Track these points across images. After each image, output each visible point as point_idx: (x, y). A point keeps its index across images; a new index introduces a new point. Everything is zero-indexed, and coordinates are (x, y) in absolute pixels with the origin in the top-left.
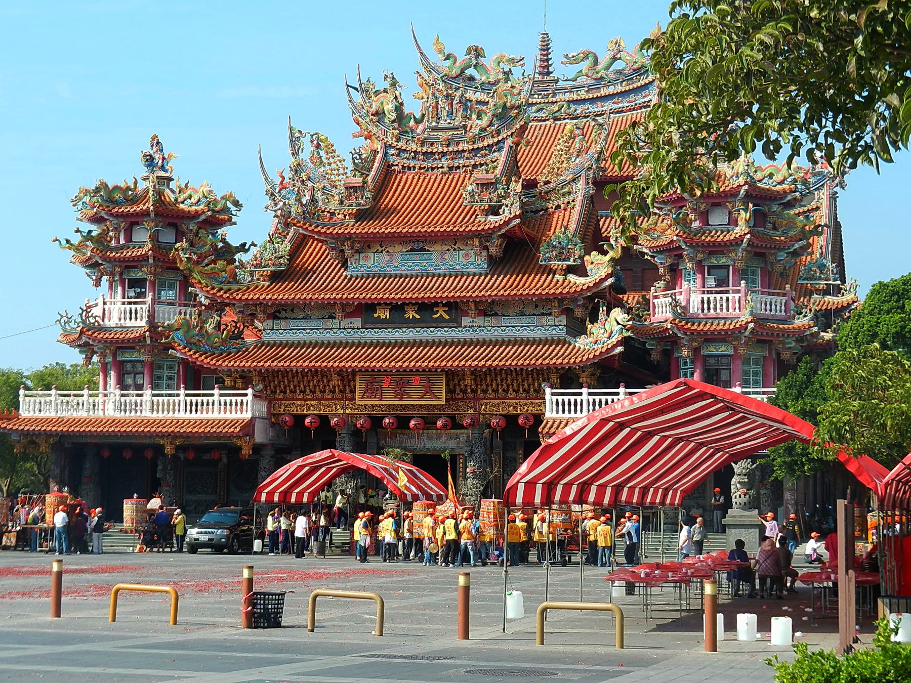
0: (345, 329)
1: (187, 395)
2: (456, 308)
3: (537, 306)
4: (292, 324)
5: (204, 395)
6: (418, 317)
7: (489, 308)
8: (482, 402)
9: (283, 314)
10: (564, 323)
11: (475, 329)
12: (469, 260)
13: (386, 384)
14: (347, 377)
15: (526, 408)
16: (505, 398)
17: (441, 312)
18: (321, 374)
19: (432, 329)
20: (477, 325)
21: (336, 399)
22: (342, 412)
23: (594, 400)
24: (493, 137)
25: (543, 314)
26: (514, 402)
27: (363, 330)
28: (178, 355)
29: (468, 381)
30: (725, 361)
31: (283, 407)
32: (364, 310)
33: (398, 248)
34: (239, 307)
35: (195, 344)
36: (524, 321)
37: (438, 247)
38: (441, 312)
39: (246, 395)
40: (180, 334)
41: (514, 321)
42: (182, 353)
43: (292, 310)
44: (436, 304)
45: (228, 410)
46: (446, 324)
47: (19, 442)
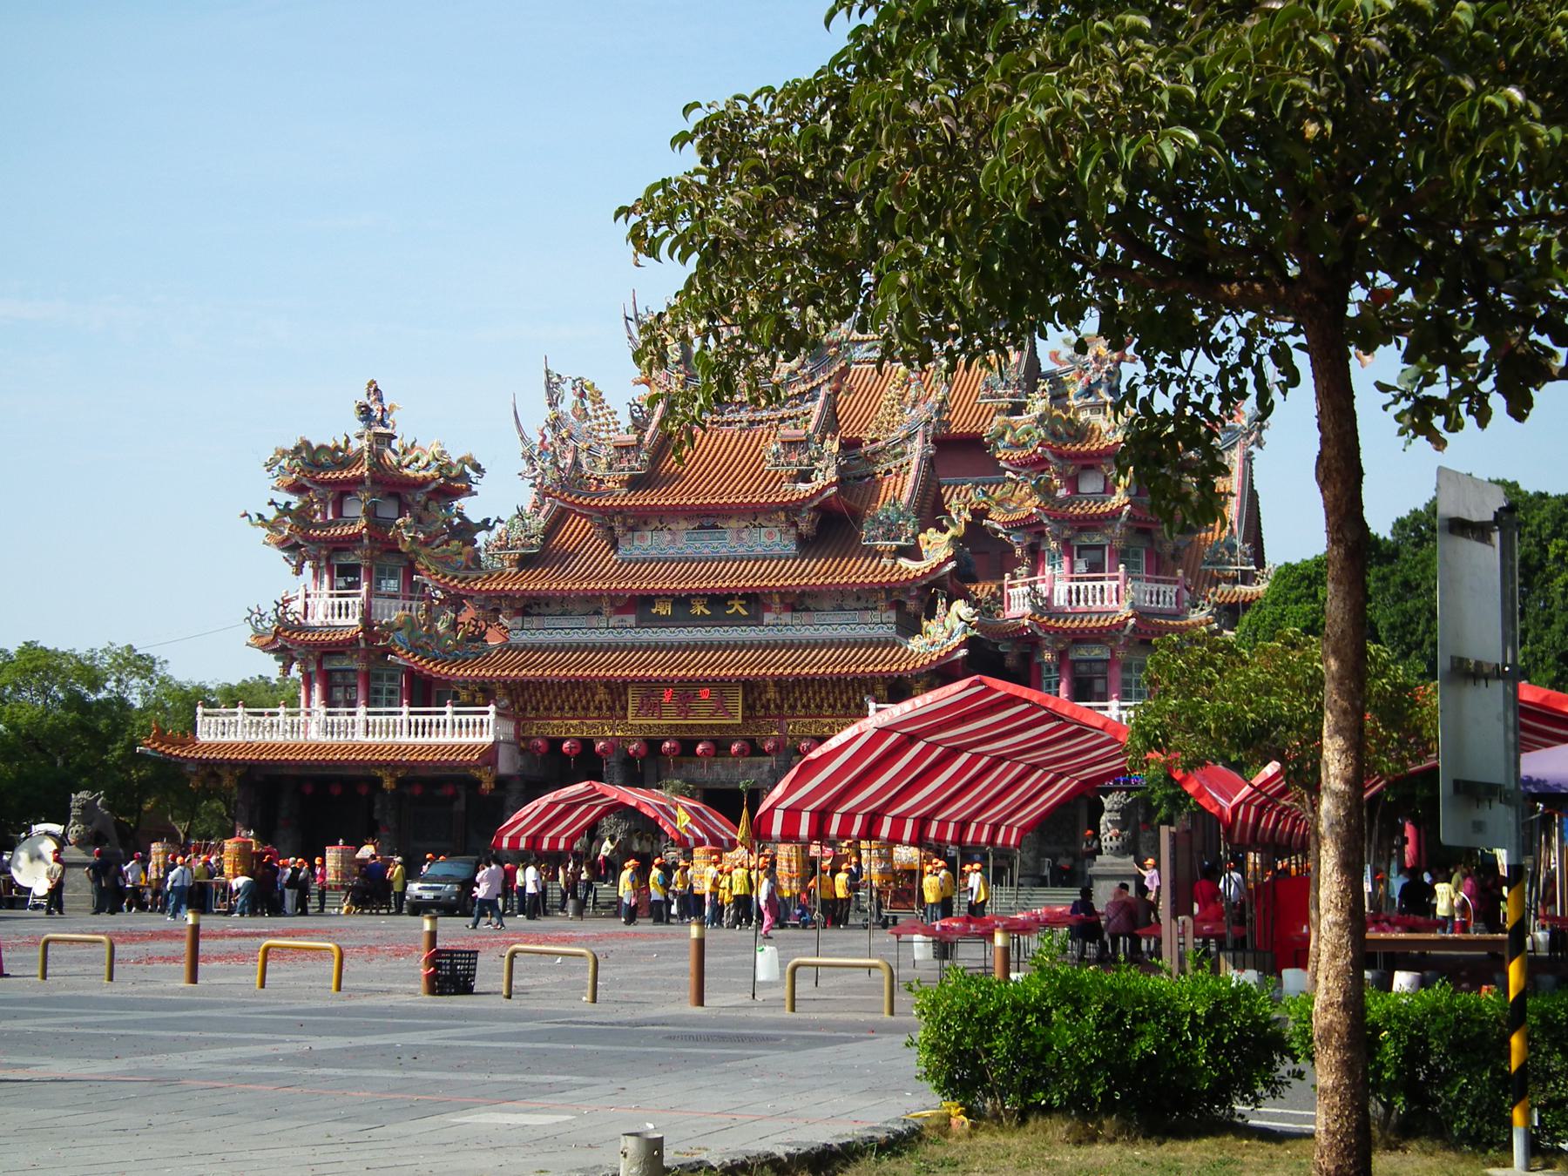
1: (412, 713)
2: (756, 601)
3: (859, 598)
4: (548, 622)
7: (798, 601)
10: (894, 619)
12: (773, 540)
17: (737, 606)
24: (805, 382)
25: (867, 609)
28: (400, 662)
29: (771, 694)
30: (1098, 667)
32: (639, 604)
33: (683, 525)
37: (733, 523)
38: (737, 606)
39: (487, 713)
40: (403, 634)
43: (547, 605)
45: (466, 732)
47: (196, 773)
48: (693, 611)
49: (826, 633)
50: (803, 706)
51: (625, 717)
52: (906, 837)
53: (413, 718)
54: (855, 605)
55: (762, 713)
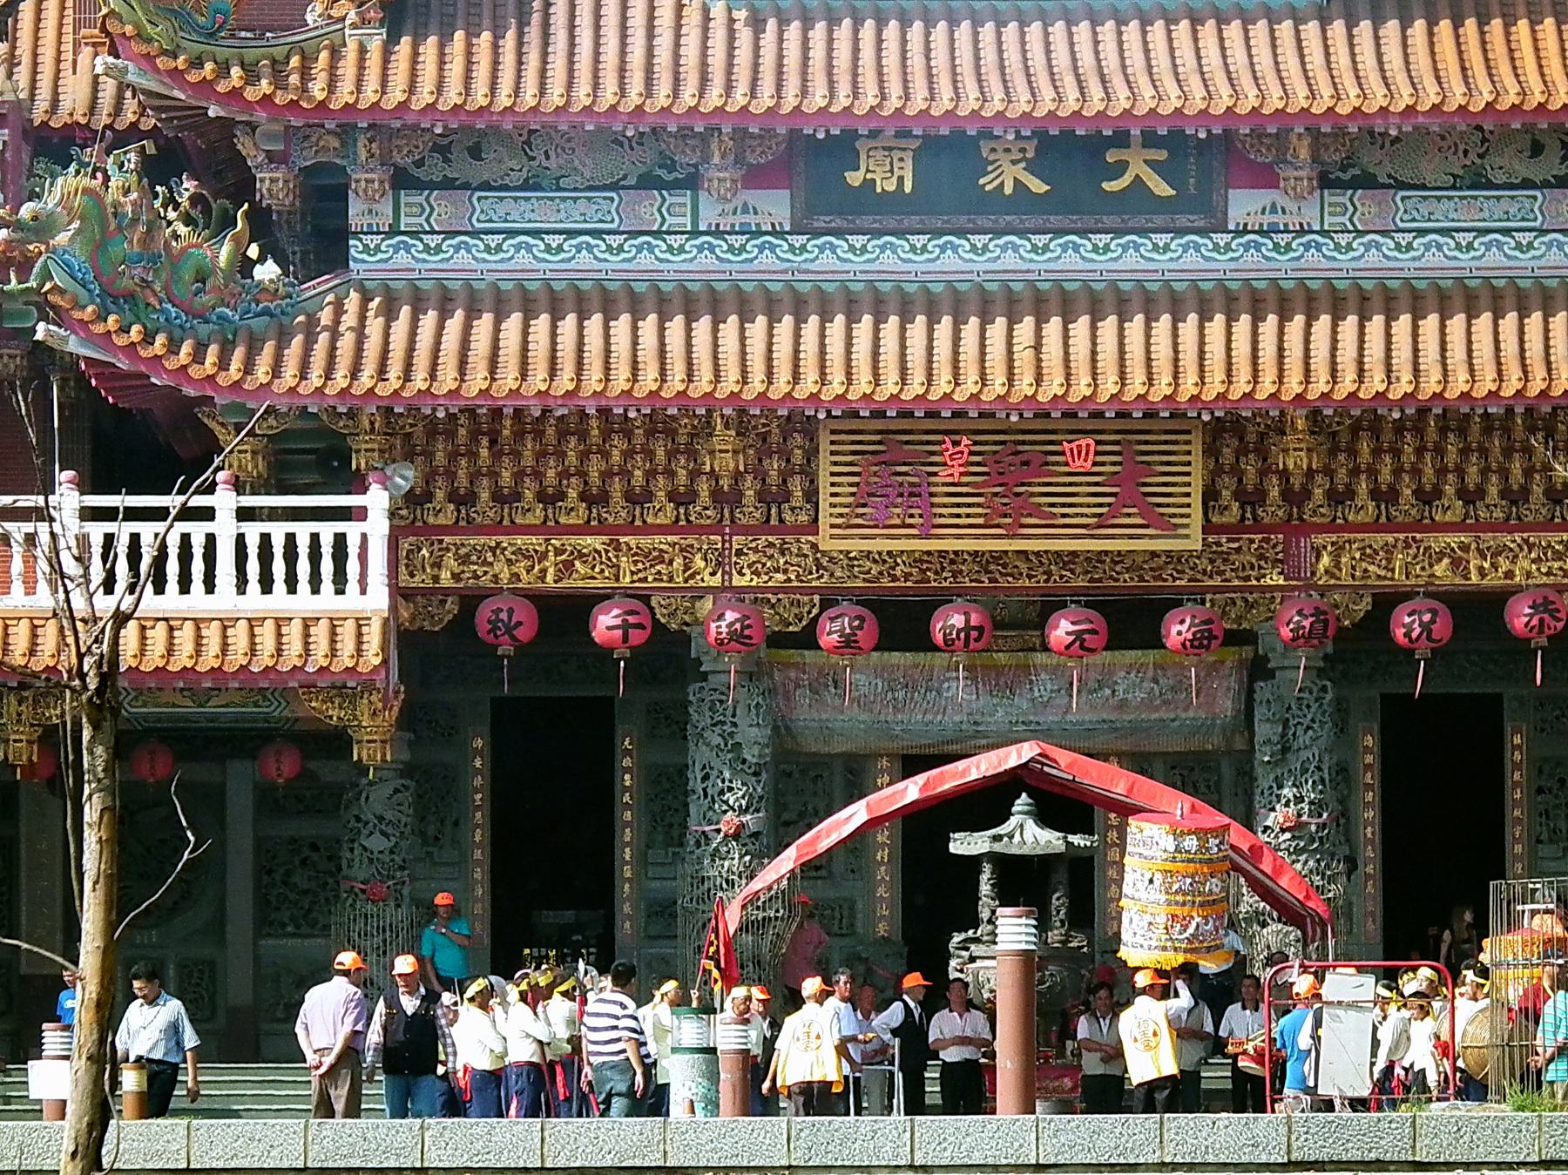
0: (718, 233)
1: (244, 514)
3: (1537, 149)
4: (484, 209)
5: (133, 514)
6: (1038, 186)
8: (1319, 540)
9: (435, 170)
11: (1282, 239)
13: (952, 467)
14: (783, 435)
15: (1504, 565)
16: (1418, 526)
17: (1138, 167)
18: (671, 427)
19: (1102, 239)
20: (1293, 222)
21: (691, 529)
22: (716, 581)
23: (265, 539)
26: (1453, 539)
27: (798, 240)
28: (74, 345)
29: (1295, 458)
31: (450, 561)
34: (270, 137)
35: (130, 297)
36: (1491, 207)
38: (1138, 167)
39: (360, 514)
41: (1450, 209)
42: (90, 339)
43: (475, 153)
44: (1121, 139)
45: (290, 599)
46: (1159, 220)
48: (988, 182)
49: (1434, 259)
50: (631, 498)
51: (813, 526)
52: (1061, 876)
53: (253, 531)
54: (1524, 168)
55: (447, 517)
